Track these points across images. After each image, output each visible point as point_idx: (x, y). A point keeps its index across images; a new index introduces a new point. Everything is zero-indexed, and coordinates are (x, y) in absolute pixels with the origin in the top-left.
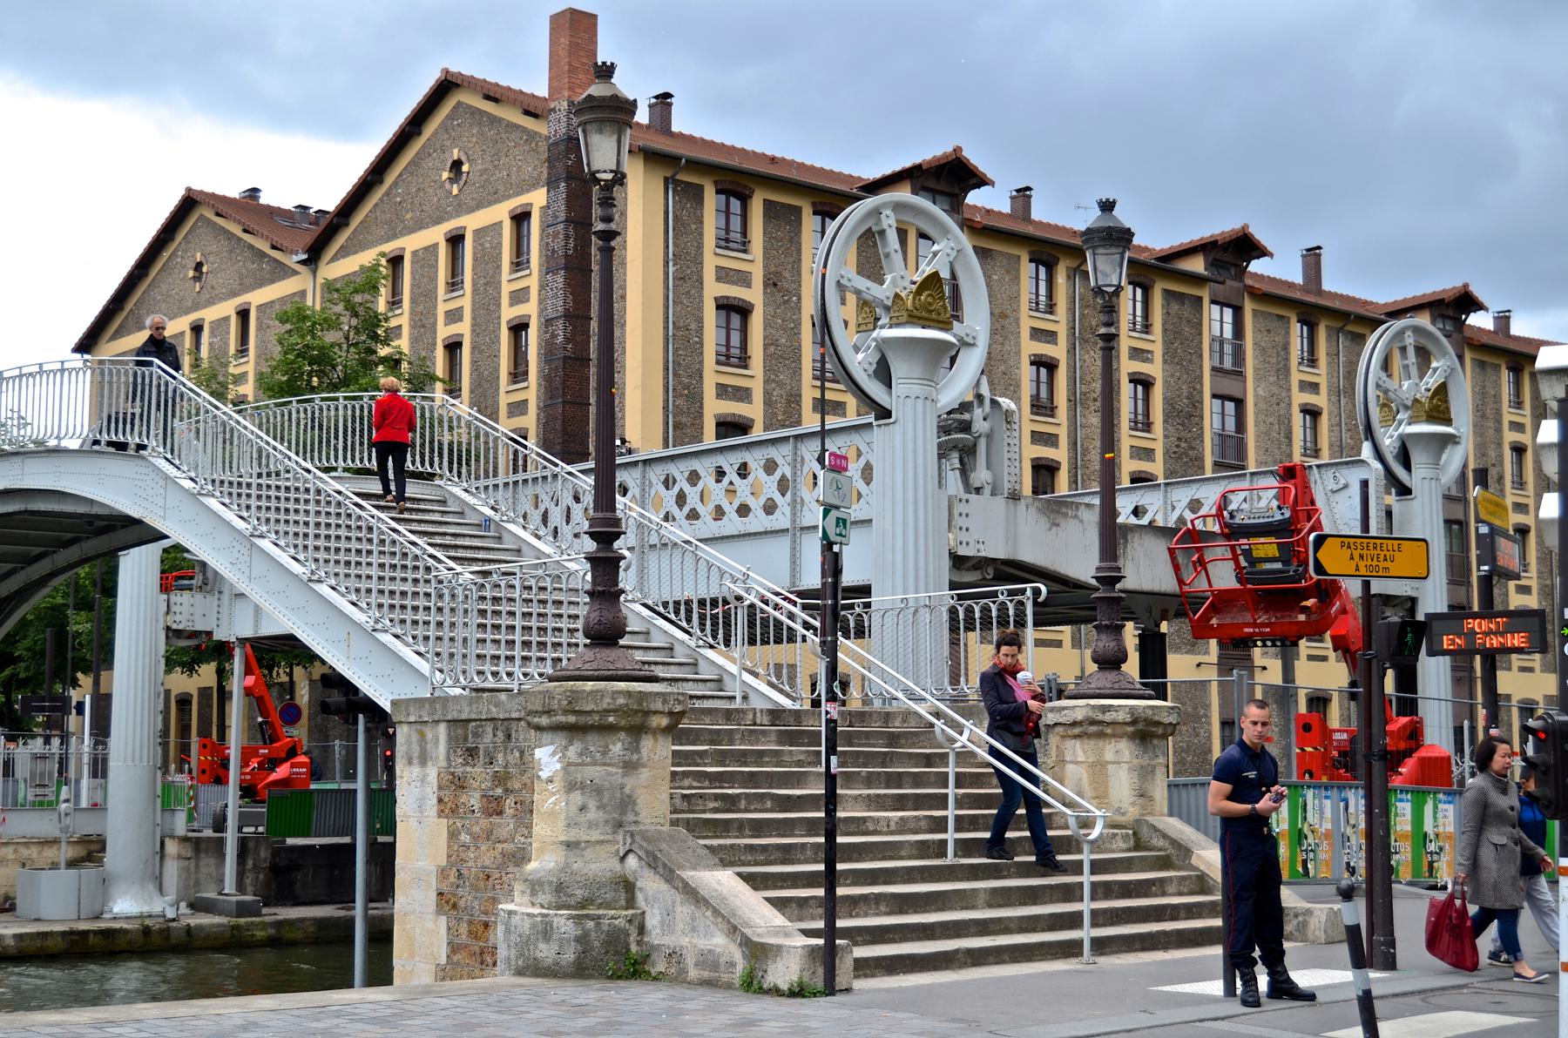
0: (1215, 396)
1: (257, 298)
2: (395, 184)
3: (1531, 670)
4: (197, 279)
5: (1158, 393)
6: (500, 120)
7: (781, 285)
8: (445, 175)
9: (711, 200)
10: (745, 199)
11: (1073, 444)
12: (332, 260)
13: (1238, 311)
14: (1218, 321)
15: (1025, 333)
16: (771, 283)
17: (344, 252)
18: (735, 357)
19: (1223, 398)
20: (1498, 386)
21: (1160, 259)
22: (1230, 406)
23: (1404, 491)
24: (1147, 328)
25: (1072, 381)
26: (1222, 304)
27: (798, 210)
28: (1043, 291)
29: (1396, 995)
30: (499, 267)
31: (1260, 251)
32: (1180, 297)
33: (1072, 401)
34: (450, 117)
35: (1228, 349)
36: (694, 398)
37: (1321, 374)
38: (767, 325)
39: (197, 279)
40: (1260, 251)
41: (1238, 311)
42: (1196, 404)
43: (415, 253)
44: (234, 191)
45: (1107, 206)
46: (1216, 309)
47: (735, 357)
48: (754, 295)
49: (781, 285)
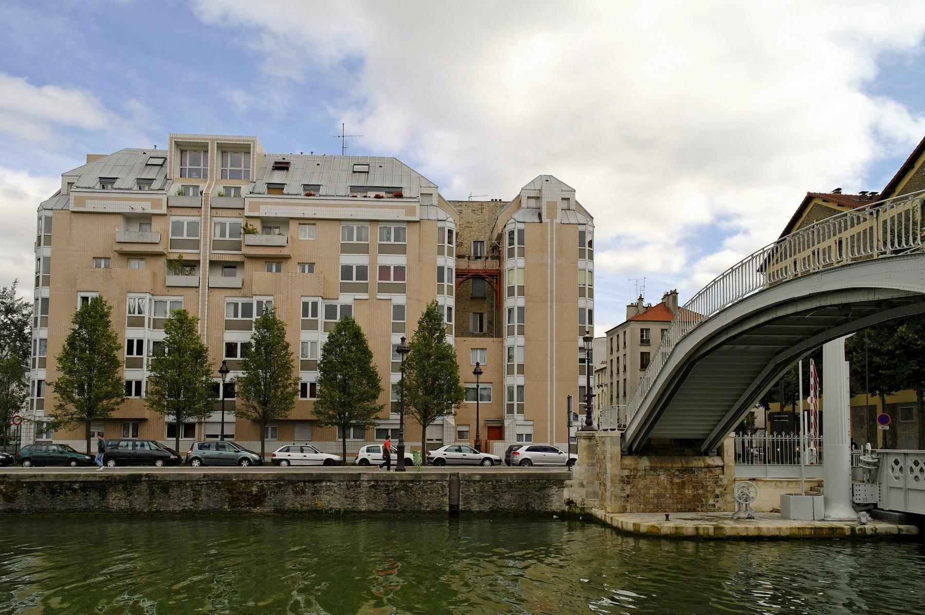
1: (845, 235)
2: (922, 167)
44: (828, 190)
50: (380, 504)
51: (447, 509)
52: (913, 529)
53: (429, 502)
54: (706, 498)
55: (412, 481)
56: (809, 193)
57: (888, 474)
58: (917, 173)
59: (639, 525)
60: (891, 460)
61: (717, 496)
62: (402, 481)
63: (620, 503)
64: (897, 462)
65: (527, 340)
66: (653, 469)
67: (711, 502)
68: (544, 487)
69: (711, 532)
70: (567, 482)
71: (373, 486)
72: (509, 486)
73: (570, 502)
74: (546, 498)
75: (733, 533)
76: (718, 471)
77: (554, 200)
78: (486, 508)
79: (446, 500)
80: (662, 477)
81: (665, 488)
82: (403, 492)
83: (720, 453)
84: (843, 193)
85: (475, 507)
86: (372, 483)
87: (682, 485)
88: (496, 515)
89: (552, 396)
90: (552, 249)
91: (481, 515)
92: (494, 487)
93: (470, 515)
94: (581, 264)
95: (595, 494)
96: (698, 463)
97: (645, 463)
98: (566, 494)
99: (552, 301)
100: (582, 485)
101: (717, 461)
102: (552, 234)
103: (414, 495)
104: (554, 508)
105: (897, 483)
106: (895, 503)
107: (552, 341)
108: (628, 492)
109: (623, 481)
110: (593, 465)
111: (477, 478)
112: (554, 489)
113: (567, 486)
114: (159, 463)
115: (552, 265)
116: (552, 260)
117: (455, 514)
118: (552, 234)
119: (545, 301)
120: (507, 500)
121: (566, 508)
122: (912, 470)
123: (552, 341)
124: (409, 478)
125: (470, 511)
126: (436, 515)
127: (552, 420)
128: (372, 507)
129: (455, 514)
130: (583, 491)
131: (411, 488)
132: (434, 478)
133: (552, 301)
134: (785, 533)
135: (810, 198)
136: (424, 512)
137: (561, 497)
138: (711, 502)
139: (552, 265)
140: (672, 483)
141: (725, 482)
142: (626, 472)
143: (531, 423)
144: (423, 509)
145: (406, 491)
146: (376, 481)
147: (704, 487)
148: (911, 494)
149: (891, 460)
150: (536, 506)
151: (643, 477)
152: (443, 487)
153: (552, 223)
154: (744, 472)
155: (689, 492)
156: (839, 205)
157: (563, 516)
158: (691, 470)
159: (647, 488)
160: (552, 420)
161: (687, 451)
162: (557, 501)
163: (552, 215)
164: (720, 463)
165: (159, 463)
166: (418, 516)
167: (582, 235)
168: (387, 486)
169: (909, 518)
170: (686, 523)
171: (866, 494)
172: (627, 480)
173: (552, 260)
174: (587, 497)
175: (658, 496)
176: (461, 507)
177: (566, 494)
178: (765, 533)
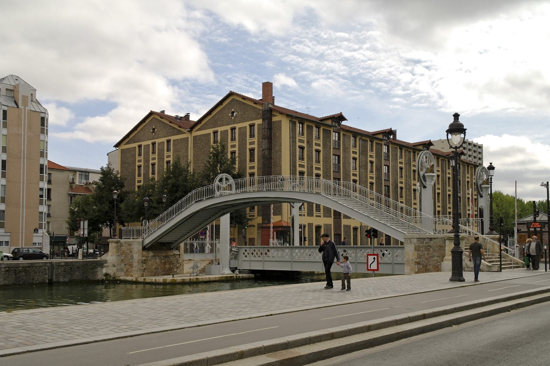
0: (333, 155)
1: (173, 138)
2: (215, 115)
3: (320, 216)
4: (153, 132)
5: (374, 164)
6: (246, 104)
7: (309, 143)
8: (230, 115)
9: (298, 125)
10: (303, 124)
11: (360, 176)
12: (196, 131)
13: (339, 134)
14: (334, 136)
15: (351, 152)
16: (308, 142)
17: (200, 129)
18: (302, 158)
19: (385, 165)
20: (397, 152)
21: (321, 120)
22: (337, 157)
23: (425, 187)
24: (303, 134)
25: (359, 162)
26: (335, 132)
27: (312, 127)
28: (301, 130)
29: (148, 333)
30: (246, 136)
31: (344, 119)
32: (363, 140)
33: (359, 167)
34: (231, 101)
35: (337, 143)
36: (295, 167)
37: (403, 160)
38: (307, 151)
39: (153, 132)
40: (344, 119)
41: (339, 134)
42: (381, 167)
43: (221, 132)
44: (158, 111)
45: (491, 164)
46: (334, 133)
47: (302, 158)
48: (305, 145)
49: (309, 143)
50: (11, 280)
51: (47, 281)
52: (252, 275)
53: (38, 278)
54: (174, 269)
55: (29, 267)
56: (151, 111)
57: (242, 257)
58: (212, 117)
59: (166, 280)
60: (243, 250)
61: (177, 268)
62: (23, 267)
63: (141, 272)
64: (246, 251)
65: (7, 181)
66: (154, 256)
67: (175, 270)
68: (94, 268)
69: (195, 280)
70: (105, 264)
71: (7, 271)
72: (78, 267)
73: (106, 275)
74: (95, 273)
75: (202, 280)
76: (178, 257)
77: (26, 95)
78: (67, 280)
79: (47, 276)
80: (158, 260)
81: (159, 265)
82: (23, 273)
83: (178, 249)
84: (166, 113)
85: (62, 280)
86: (7, 269)
87: (165, 263)
88: (72, 283)
89: (23, 217)
90: (24, 125)
91: (65, 284)
92: (71, 268)
93: (59, 283)
94: (42, 137)
95: (122, 270)
96: (170, 253)
97: (151, 254)
98: (104, 271)
99: (24, 158)
100: (114, 266)
101: (176, 252)
102: (25, 116)
103: (30, 275)
104: (98, 278)
105: (246, 259)
106: (246, 266)
107: (23, 183)
108: (144, 267)
109: (142, 262)
110: (119, 256)
111: (63, 264)
112: (99, 268)
113: (105, 267)
114: (21, 259)
115: (24, 135)
116: (25, 133)
117: (51, 283)
118: (25, 116)
119: (20, 158)
120: (77, 275)
121: (104, 278)
122: (244, 254)
123: (23, 183)
124: (28, 265)
125: (59, 282)
126: (41, 285)
127: (22, 232)
128: (6, 282)
129: (51, 283)
130: (115, 269)
131: (28, 271)
132: (41, 265)
133: (24, 158)
134: (217, 279)
135: (151, 113)
136: (35, 284)
137: (102, 272)
138: (175, 270)
139: (24, 135)
140: (161, 262)
141: (180, 261)
142: (144, 258)
143: (9, 234)
144: (35, 282)
145: (25, 272)
146: (9, 268)
147: (173, 264)
148: (252, 262)
149: (243, 250)
150: (90, 277)
151: (150, 260)
152: (45, 269)
153: (25, 109)
154: (187, 257)
155: (167, 266)
156: (179, 127)
157: (102, 282)
158: (167, 257)
159: (152, 265)
160: (22, 232)
161: (164, 248)
162: (101, 273)
163: (25, 104)
164: (179, 253)
165: (21, 259)
166: (30, 285)
167: (43, 119)
168: (15, 270)
169: (253, 272)
170: (169, 278)
171: (234, 264)
172: (144, 262)
173: (25, 133)
174: (117, 271)
175: (156, 268)
176: (54, 280)
177: (104, 271)
178: (212, 280)
